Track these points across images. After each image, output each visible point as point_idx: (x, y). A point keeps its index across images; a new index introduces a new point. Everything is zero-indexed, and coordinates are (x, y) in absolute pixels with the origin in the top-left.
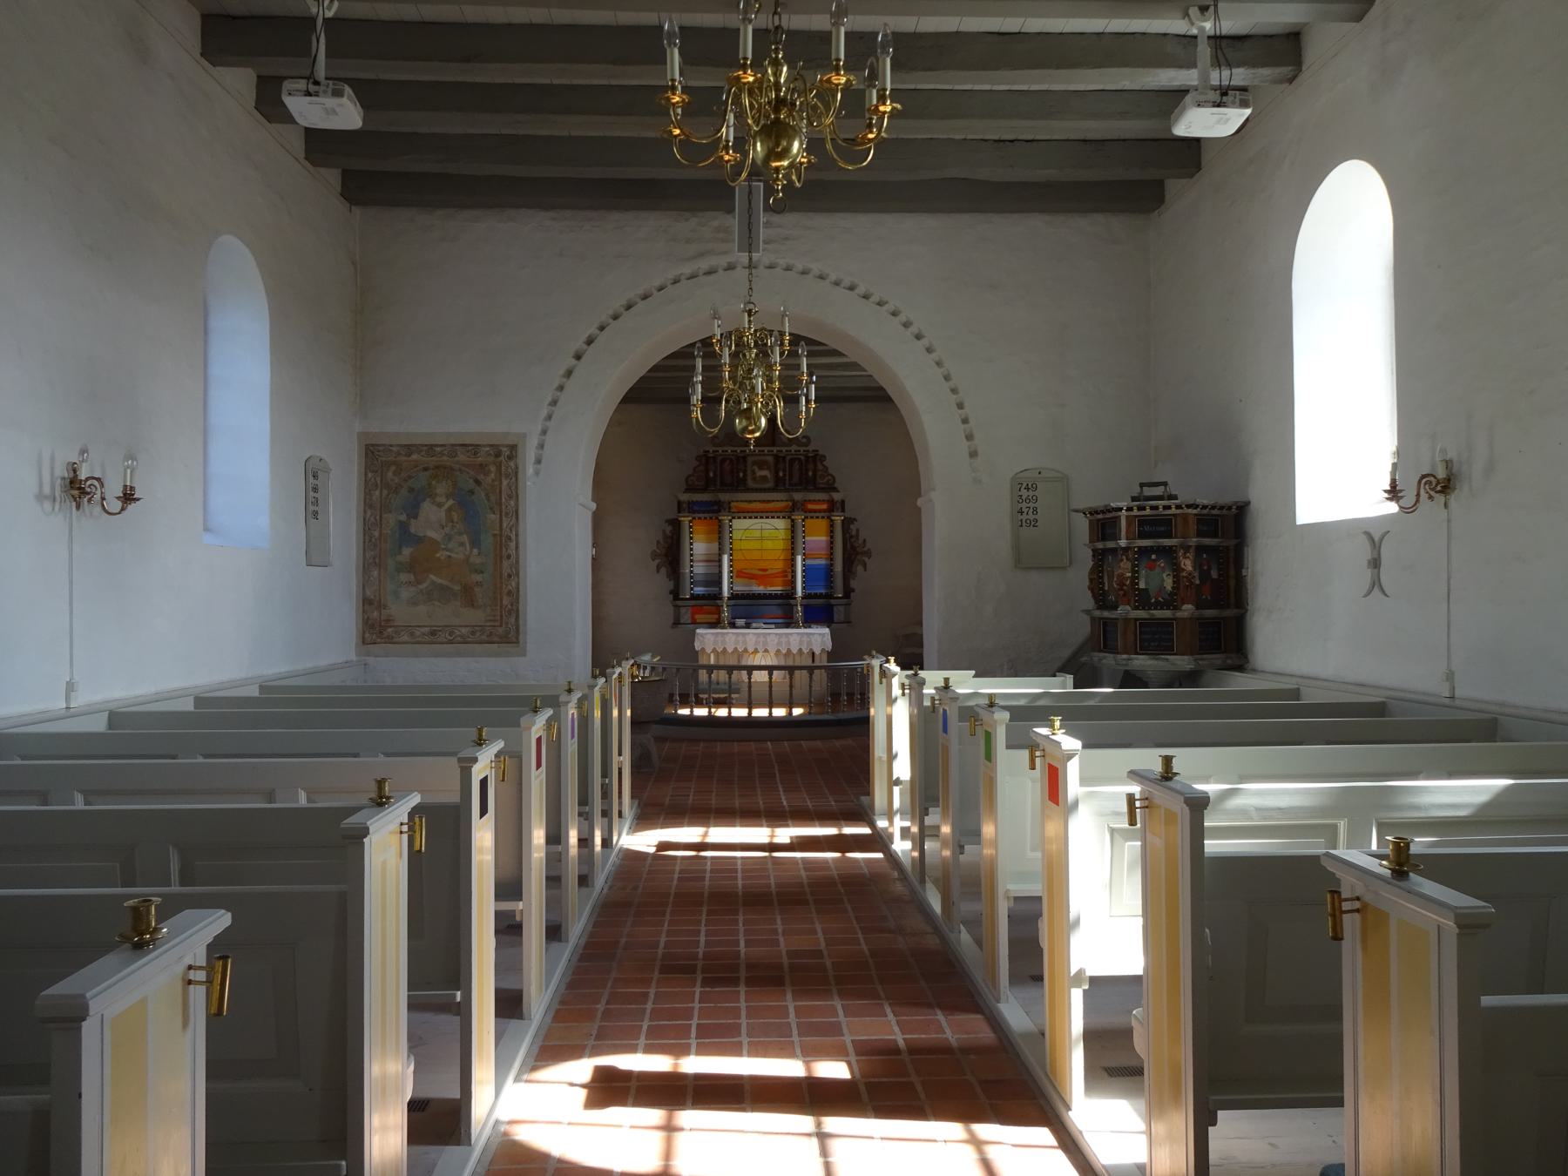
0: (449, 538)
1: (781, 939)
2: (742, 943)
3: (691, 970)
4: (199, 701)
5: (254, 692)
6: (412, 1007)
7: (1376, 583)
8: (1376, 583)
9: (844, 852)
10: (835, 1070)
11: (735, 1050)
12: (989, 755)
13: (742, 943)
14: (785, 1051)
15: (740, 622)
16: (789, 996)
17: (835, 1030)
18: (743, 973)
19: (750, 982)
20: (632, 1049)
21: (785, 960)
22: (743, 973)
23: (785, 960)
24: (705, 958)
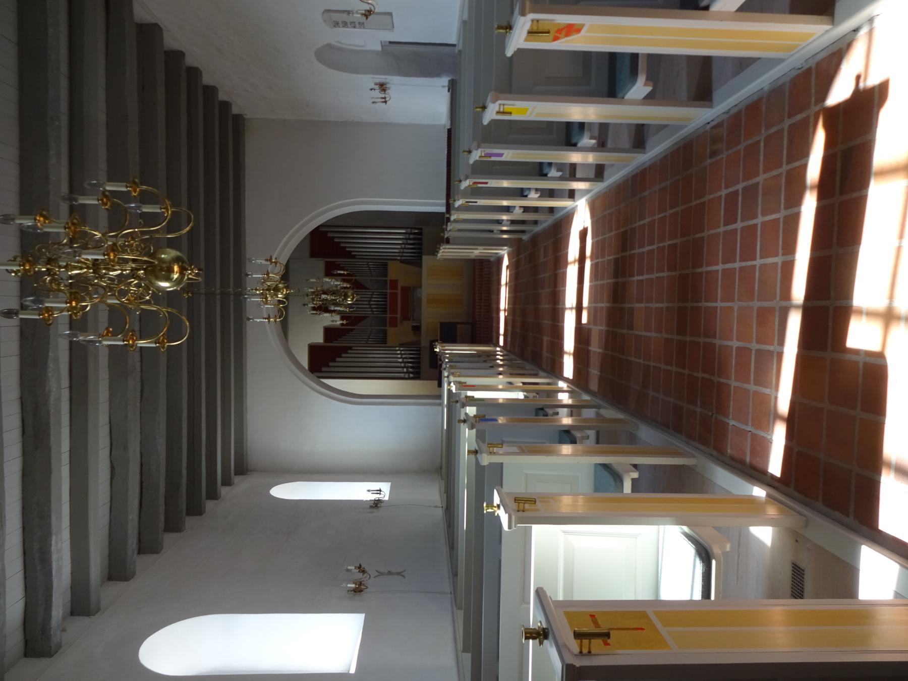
0: (540, 635)
1: (642, 305)
2: (640, 278)
3: (681, 331)
4: (465, 650)
5: (460, 614)
6: (613, 56)
7: (399, 574)
8: (399, 574)
9: (791, 421)
10: (584, 320)
11: (591, 281)
12: (512, 13)
13: (640, 278)
14: (590, 302)
15: (392, 242)
16: (608, 305)
17: (595, 324)
18: (620, 280)
19: (616, 285)
20: (593, 238)
21: (627, 306)
22: (620, 280)
23: (627, 306)
24: (719, 383)
